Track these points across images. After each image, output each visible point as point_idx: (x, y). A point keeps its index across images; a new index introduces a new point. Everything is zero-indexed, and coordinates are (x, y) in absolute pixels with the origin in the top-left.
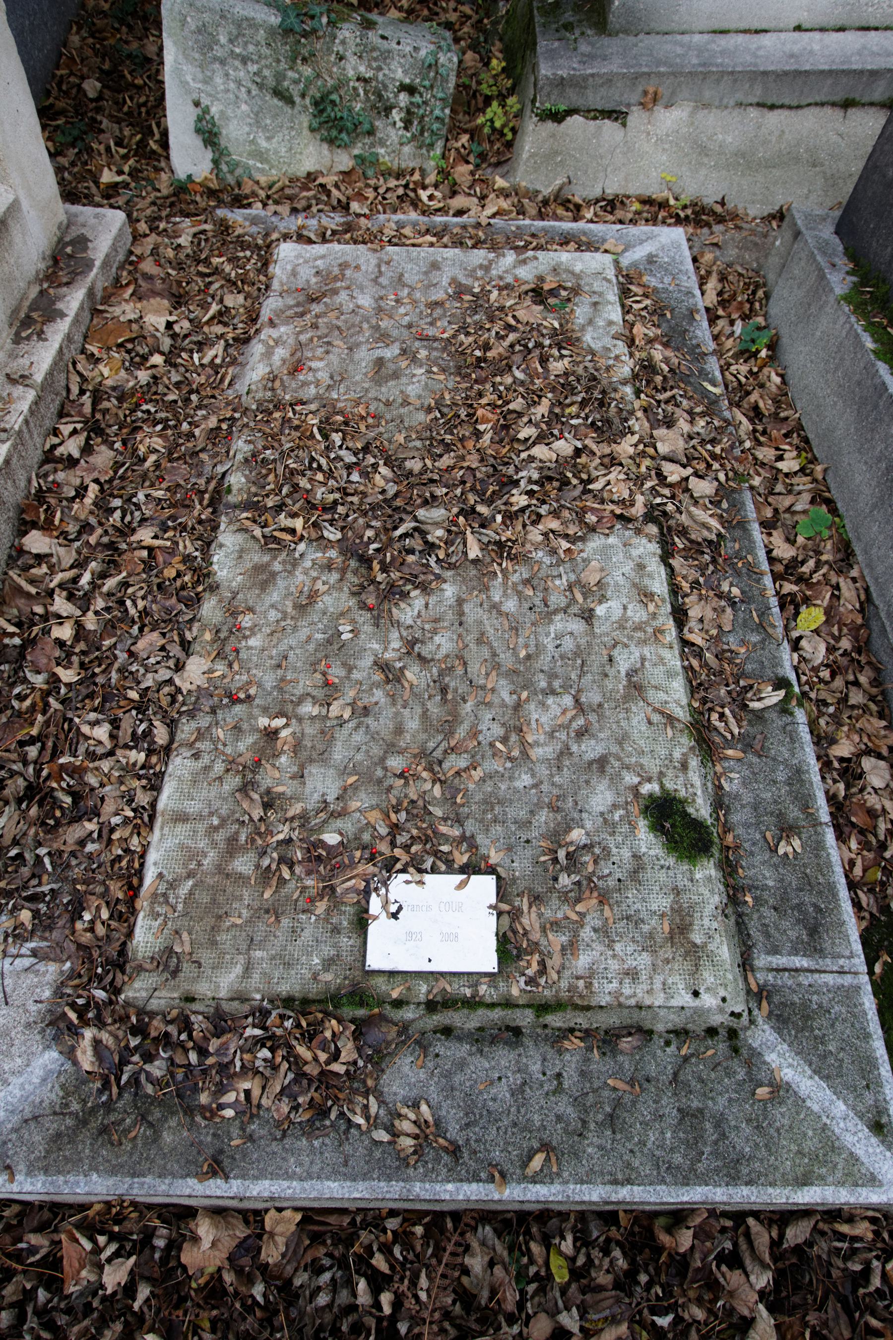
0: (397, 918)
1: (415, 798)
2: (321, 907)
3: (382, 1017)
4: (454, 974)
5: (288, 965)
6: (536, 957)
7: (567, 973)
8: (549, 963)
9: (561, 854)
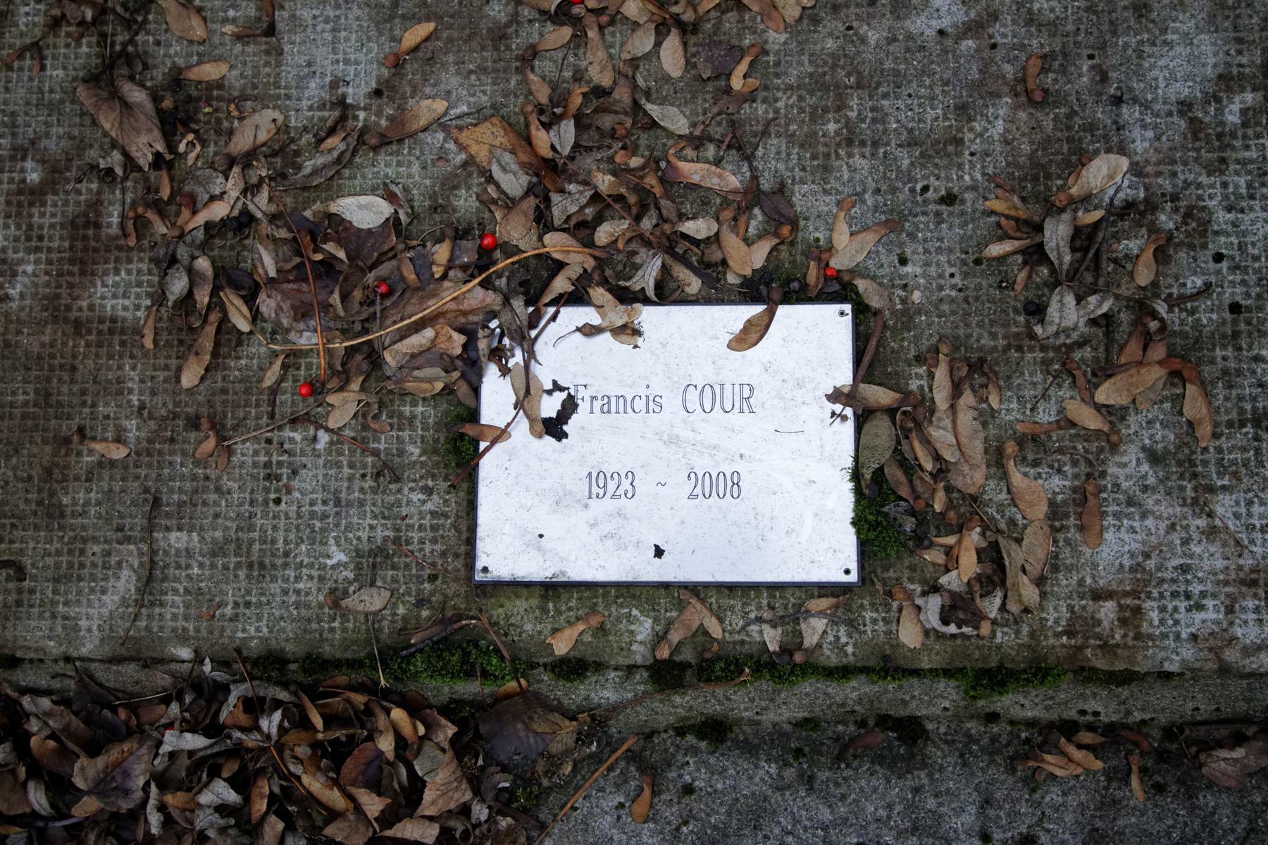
0: (560, 435)
1: (606, 81)
2: (343, 407)
3: (533, 702)
4: (731, 588)
5: (260, 569)
6: (974, 537)
7: (1066, 582)
8: (1014, 555)
9: (1057, 234)
